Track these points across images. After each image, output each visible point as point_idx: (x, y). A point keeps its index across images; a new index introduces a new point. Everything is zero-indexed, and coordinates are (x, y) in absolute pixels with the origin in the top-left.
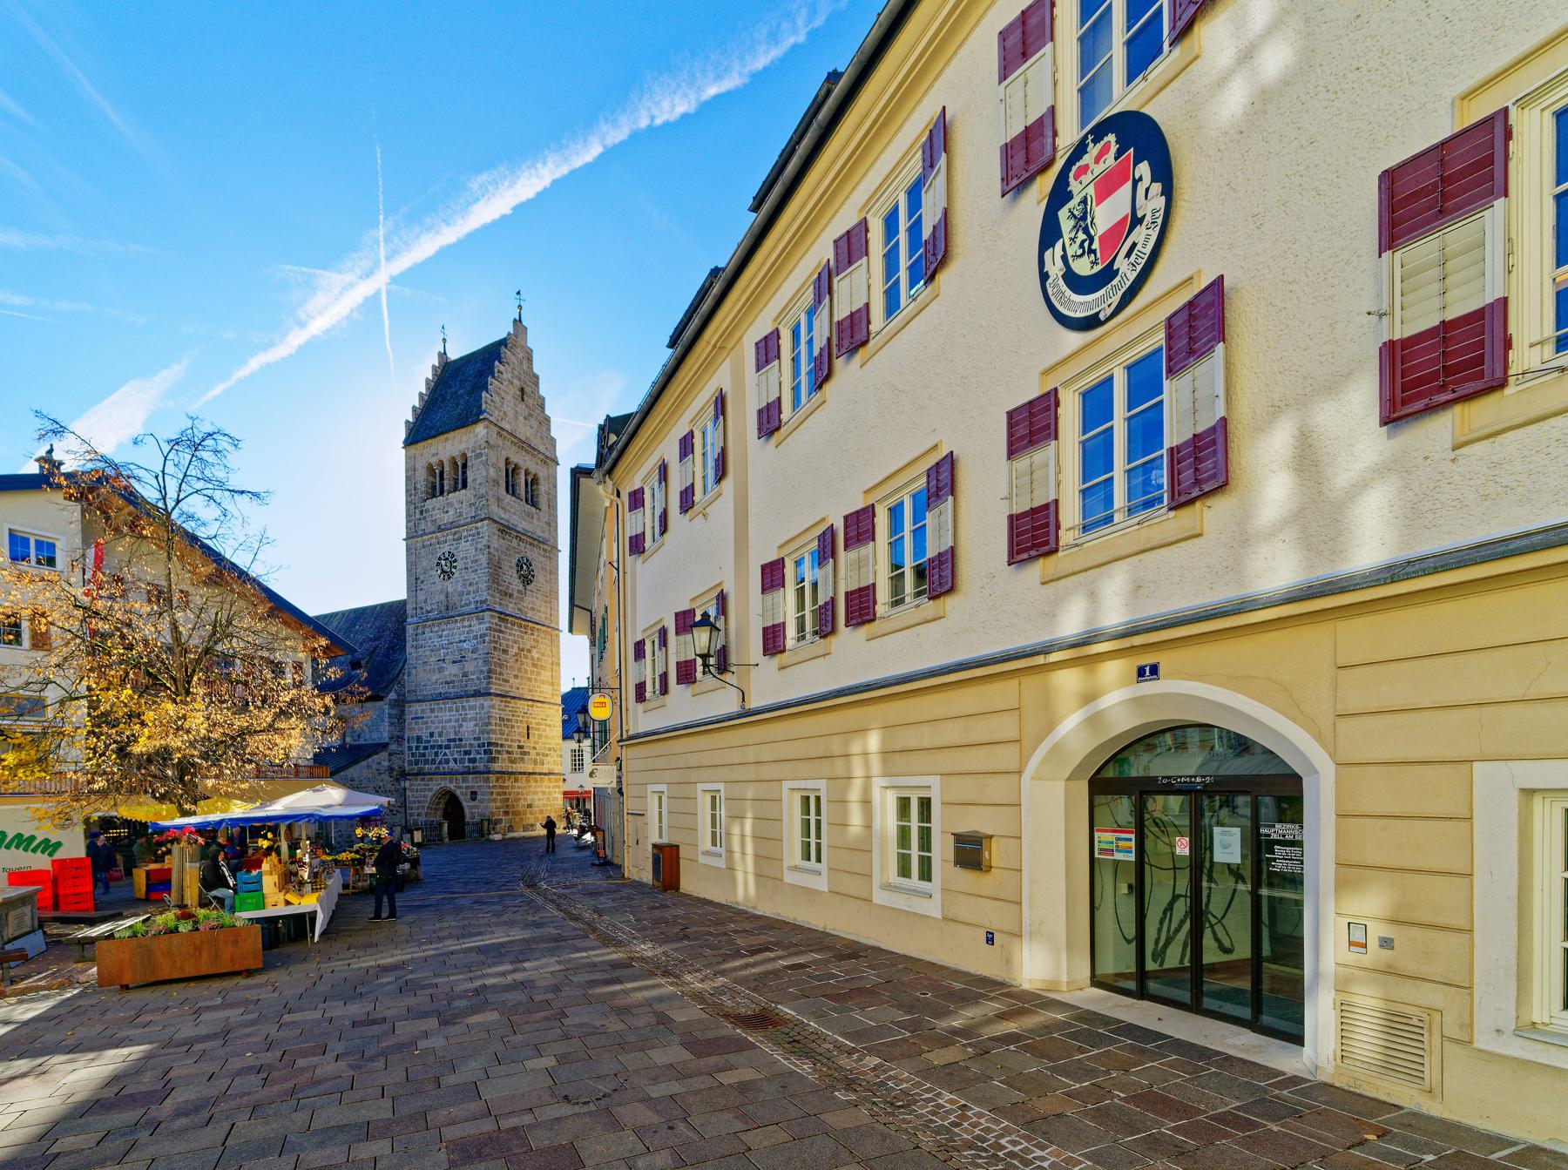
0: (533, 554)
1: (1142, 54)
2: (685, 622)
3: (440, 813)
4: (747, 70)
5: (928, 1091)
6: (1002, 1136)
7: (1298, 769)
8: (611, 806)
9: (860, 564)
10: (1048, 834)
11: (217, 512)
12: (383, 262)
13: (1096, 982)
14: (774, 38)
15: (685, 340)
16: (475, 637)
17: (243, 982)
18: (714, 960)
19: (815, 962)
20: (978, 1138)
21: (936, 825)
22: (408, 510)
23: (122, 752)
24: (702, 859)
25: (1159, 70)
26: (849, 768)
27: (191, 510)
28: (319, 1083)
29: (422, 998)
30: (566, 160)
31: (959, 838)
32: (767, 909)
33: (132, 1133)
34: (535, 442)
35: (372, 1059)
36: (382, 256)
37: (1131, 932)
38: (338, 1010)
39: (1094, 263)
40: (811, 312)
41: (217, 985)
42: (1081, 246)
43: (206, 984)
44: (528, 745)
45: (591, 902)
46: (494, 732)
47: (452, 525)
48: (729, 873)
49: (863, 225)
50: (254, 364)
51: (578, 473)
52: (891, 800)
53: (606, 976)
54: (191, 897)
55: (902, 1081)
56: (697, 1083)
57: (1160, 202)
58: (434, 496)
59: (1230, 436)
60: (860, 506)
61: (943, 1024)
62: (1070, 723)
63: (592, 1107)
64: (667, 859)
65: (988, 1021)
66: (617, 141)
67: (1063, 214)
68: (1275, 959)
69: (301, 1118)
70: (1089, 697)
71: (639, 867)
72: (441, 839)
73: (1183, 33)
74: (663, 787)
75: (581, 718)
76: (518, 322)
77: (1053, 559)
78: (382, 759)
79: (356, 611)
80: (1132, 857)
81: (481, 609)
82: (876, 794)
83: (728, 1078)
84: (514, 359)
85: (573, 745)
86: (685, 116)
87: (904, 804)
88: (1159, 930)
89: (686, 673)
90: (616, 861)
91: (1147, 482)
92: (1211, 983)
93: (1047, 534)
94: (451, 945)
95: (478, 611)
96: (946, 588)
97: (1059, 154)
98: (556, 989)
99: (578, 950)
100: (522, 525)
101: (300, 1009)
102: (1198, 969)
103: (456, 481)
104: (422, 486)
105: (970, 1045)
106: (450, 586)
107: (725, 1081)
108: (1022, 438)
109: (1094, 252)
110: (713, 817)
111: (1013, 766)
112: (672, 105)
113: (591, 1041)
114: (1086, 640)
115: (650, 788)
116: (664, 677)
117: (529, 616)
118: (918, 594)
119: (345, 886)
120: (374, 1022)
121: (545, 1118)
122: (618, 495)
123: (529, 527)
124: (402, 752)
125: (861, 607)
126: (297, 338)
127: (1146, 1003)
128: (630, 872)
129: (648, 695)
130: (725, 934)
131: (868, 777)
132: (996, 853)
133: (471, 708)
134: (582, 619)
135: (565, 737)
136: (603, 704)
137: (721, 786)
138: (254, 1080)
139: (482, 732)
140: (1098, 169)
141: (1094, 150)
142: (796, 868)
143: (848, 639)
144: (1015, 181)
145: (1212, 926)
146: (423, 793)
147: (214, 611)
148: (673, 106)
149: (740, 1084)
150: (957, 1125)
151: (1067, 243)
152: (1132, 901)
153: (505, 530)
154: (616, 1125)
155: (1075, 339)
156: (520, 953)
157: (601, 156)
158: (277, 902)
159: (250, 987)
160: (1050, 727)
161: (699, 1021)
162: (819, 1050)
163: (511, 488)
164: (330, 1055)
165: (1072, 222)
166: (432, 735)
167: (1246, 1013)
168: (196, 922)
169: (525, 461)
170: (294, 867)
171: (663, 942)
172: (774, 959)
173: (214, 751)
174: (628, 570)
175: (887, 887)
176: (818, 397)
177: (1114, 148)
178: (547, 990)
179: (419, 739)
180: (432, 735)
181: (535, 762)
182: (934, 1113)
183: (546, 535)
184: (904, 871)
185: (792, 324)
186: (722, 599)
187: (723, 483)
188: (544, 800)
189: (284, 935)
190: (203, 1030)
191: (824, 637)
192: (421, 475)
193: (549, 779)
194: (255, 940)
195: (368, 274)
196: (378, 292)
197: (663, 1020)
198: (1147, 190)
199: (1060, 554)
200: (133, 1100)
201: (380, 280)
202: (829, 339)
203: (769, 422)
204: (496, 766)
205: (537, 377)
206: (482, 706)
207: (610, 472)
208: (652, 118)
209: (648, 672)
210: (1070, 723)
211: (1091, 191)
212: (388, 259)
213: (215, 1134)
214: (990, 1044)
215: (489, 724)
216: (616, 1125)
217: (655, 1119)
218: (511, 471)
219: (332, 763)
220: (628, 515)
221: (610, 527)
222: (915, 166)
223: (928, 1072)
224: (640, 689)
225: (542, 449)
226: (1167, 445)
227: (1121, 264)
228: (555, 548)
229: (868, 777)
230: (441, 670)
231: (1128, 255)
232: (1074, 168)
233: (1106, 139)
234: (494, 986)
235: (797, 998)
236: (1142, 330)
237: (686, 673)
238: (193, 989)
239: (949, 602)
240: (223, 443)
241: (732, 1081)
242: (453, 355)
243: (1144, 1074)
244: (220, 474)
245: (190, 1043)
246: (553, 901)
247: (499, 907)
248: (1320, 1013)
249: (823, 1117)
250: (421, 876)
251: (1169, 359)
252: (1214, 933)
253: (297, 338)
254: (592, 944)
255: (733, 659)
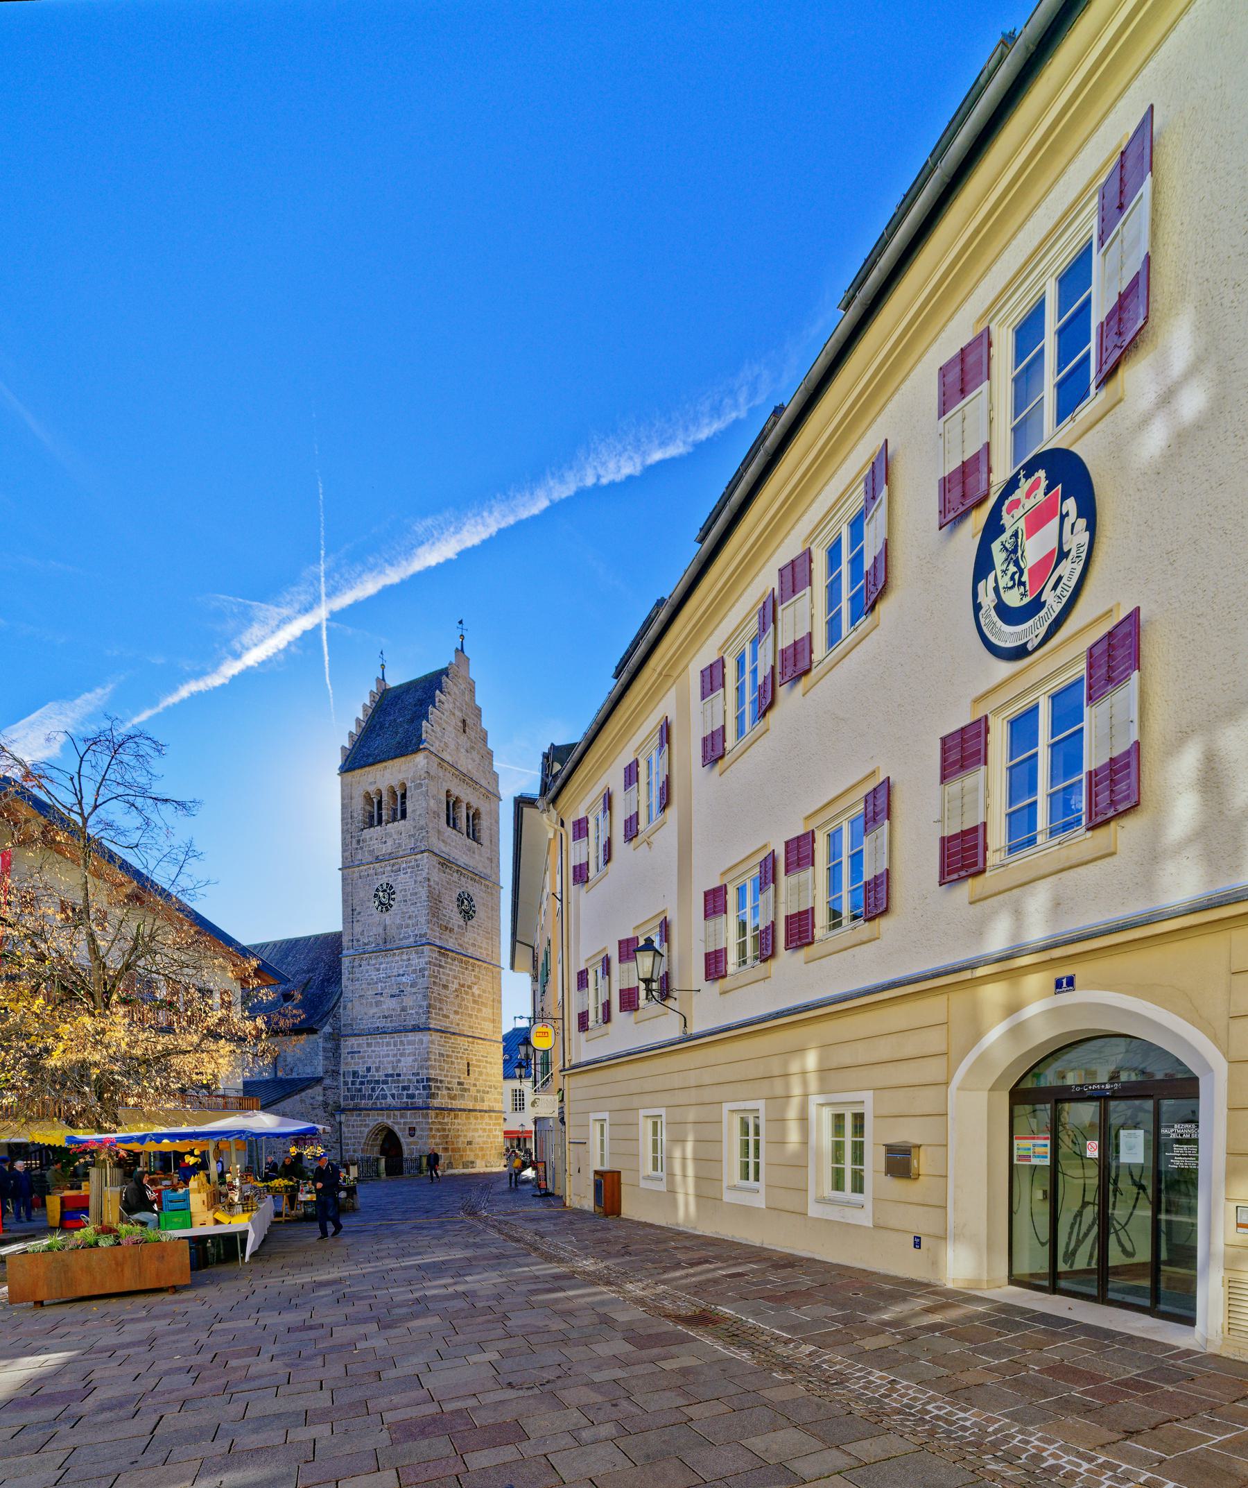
0: (474, 890)
1: (1071, 395)
2: (629, 949)
3: (377, 1149)
4: (691, 439)
5: (860, 1370)
6: (929, 1403)
7: (1197, 1072)
8: (553, 1139)
9: (800, 888)
10: (972, 1142)
11: (139, 821)
12: (323, 598)
13: (1013, 1280)
14: (717, 411)
15: (631, 670)
16: (414, 971)
17: (168, 1297)
18: (653, 1271)
19: (753, 1271)
20: (907, 1406)
21: (868, 1138)
22: (344, 839)
23: (35, 1065)
24: (643, 1184)
25: (1086, 411)
26: (787, 1086)
27: (111, 817)
28: (253, 1379)
29: (362, 1306)
30: (513, 511)
31: (891, 1149)
32: (707, 1229)
33: (50, 1426)
34: (476, 775)
35: (309, 1358)
36: (323, 590)
37: (1045, 1235)
38: (270, 1318)
39: (1023, 595)
40: (756, 641)
41: (140, 1301)
42: (1012, 578)
43: (128, 1300)
44: (468, 1082)
45: (532, 1226)
46: (433, 1067)
47: (391, 857)
48: (672, 1197)
49: (807, 555)
50: (184, 692)
51: (522, 803)
52: (827, 1115)
53: (547, 1286)
54: (112, 1212)
55: (835, 1364)
56: (640, 1370)
57: (1084, 537)
58: (371, 826)
59: (1143, 760)
60: (800, 831)
61: (873, 1318)
62: (995, 1033)
63: (536, 1391)
64: (608, 1187)
65: (916, 1315)
66: (563, 496)
67: (996, 547)
68: (1169, 1263)
69: (235, 1409)
70: (1013, 1008)
71: (580, 1195)
72: (378, 1175)
73: (1108, 377)
74: (605, 1115)
75: (523, 1049)
76: (460, 651)
77: (981, 879)
78: (316, 1092)
79: (289, 941)
80: (1047, 1162)
81: (420, 943)
82: (813, 1110)
83: (668, 1365)
84: (455, 689)
85: (515, 1084)
86: (630, 478)
87: (839, 1118)
88: (1071, 1234)
89: (629, 1000)
90: (557, 1192)
91: (1067, 803)
92: (1114, 1282)
93: (976, 855)
94: (391, 1263)
95: (417, 945)
96: (881, 909)
97: (993, 490)
98: (499, 1297)
99: (520, 1266)
100: (463, 859)
101: (231, 1319)
102: (1103, 1271)
103: (395, 811)
104: (359, 815)
105: (898, 1333)
106: (387, 918)
107: (667, 1367)
108: (954, 763)
109: (1023, 584)
110: (655, 1142)
111: (941, 1079)
112: (620, 467)
113: (534, 1339)
114: (1013, 961)
115: (593, 1116)
116: (607, 1006)
117: (470, 951)
118: (855, 917)
119: (278, 1214)
120: (311, 1328)
121: (488, 1401)
122: (562, 825)
123: (471, 863)
124: (337, 1087)
125: (800, 930)
126: (232, 669)
127: (1057, 1297)
128: (572, 1201)
129: (591, 1024)
130: (665, 1250)
131: (806, 1096)
132: (923, 1162)
133: (409, 1043)
134: (524, 955)
135: (507, 1077)
136: (545, 1034)
137: (662, 1111)
138: (187, 1379)
139: (421, 1067)
140: (1029, 504)
141: (1025, 485)
142: (734, 1188)
143: (785, 958)
144: (952, 518)
145: (1116, 1232)
146: (359, 1132)
147: (135, 925)
148: (619, 469)
149: (681, 1369)
150: (887, 1396)
151: (999, 574)
152: (1046, 1207)
153: (445, 863)
154: (562, 1405)
155: (1005, 669)
156: (462, 1269)
157: (546, 511)
158: (205, 1220)
159: (176, 1302)
160: (978, 1036)
161: (641, 1320)
162: (757, 1342)
163: (452, 821)
164: (265, 1356)
165: (1004, 555)
166: (369, 1069)
167: (1147, 1303)
168: (117, 1237)
169: (466, 794)
170: (224, 1189)
171: (609, 1255)
172: (714, 1270)
173: (138, 1066)
174: (572, 900)
175: (821, 1201)
176: (761, 725)
177: (1044, 484)
178: (488, 1298)
179: (355, 1074)
180: (369, 1069)
181: (476, 1099)
182: (865, 1388)
183: (488, 871)
184: (838, 1185)
185: (736, 653)
186: (665, 927)
187: (667, 811)
188: (484, 1148)
189: (216, 1254)
190: (126, 1338)
191: (764, 961)
192: (358, 804)
193: (486, 1123)
194: (184, 1257)
195: (307, 609)
196: (318, 627)
197: (606, 1321)
198: (1073, 525)
199: (987, 874)
200: (51, 1399)
201: (321, 614)
202: (773, 668)
203: (713, 750)
204: (436, 1103)
205: (480, 710)
206: (421, 1042)
207: (554, 801)
208: (599, 477)
209: (591, 1001)
210: (995, 1033)
211: (1022, 524)
212: (328, 595)
213: (144, 1424)
214: (917, 1332)
215: (428, 1059)
216: (562, 1405)
217: (599, 1398)
218: (452, 805)
219: (263, 1093)
220: (572, 843)
221: (554, 860)
222: (857, 499)
223: (861, 1355)
224: (583, 1019)
225: (484, 783)
226: (1086, 767)
227: (1048, 596)
228: (497, 884)
229: (806, 1096)
230: (378, 1004)
231: (1055, 588)
232: (1007, 502)
233: (1037, 475)
234: (434, 1296)
235: (736, 1300)
236: (1066, 660)
237: (629, 1000)
238: (114, 1305)
239: (883, 924)
240: (146, 748)
241: (675, 1366)
242: (393, 681)
243: (1054, 1353)
244: (143, 780)
245: (112, 1351)
246: (494, 1226)
247: (438, 1232)
248: (1210, 1292)
249: (761, 1393)
250: (358, 1206)
251: (1090, 687)
252: (1117, 1235)
253: (232, 669)
254: (534, 1260)
255: (675, 984)
